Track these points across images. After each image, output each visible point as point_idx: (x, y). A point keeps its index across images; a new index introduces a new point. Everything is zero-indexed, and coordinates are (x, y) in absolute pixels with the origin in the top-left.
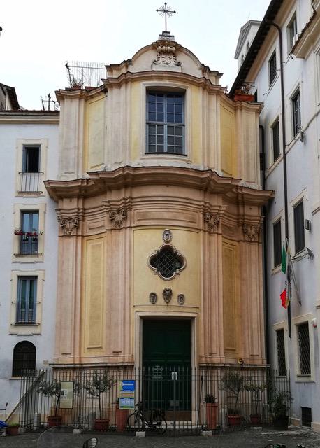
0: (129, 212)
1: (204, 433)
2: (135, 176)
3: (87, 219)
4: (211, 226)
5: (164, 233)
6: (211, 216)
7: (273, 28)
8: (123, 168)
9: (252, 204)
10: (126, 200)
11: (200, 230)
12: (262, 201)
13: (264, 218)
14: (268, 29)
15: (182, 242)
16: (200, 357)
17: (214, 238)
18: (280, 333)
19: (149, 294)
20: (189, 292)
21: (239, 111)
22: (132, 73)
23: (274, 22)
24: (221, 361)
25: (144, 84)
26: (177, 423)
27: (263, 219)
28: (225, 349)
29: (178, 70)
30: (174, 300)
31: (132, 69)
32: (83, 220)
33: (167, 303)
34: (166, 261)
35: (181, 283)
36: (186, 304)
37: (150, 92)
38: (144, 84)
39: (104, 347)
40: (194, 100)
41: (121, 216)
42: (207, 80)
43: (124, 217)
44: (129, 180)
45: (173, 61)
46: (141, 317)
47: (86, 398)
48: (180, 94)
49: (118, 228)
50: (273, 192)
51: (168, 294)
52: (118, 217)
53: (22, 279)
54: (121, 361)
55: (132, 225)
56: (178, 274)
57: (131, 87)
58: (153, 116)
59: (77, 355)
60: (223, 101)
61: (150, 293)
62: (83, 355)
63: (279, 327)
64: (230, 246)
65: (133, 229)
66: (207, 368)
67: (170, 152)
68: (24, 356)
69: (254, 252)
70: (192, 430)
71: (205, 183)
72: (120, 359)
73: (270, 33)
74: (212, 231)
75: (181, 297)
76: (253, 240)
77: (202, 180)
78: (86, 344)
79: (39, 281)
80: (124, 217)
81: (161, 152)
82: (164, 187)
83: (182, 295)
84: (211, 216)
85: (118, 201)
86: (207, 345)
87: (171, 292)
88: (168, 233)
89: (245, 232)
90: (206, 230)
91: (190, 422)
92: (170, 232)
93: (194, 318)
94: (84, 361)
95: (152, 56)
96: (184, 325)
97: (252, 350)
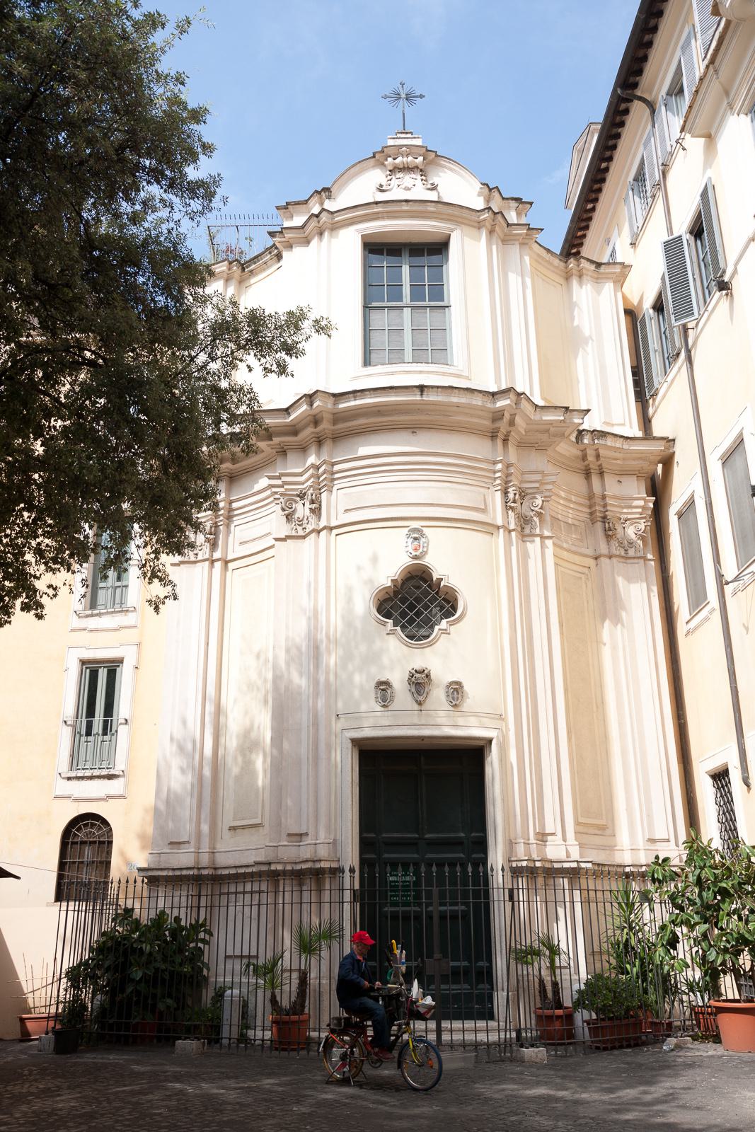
0: (324, 496)
1: (528, 1052)
2: (338, 418)
3: (236, 520)
4: (524, 521)
5: (408, 536)
6: (522, 498)
7: (637, 108)
8: (310, 398)
9: (623, 473)
10: (318, 468)
11: (498, 528)
12: (494, 247)
13: (656, 503)
14: (626, 112)
15: (449, 560)
16: (511, 844)
17: (534, 547)
18: (721, 777)
19: (373, 684)
20: (479, 679)
21: (575, 282)
22: (332, 213)
23: (638, 93)
24: (568, 855)
25: (358, 231)
26: (445, 1024)
27: (651, 505)
28: (577, 823)
29: (432, 196)
30: (438, 695)
31: (330, 205)
32: (228, 526)
33: (420, 703)
34: (416, 602)
35: (450, 653)
36: (468, 705)
37: (373, 247)
38: (358, 231)
39: (266, 824)
40: (469, 258)
41: (308, 505)
42: (495, 214)
43: (313, 506)
44: (325, 426)
45: (419, 182)
46: (355, 742)
47: (226, 957)
48: (439, 248)
49: (301, 533)
50: (671, 441)
51: (420, 683)
52: (302, 510)
53: (91, 669)
54: (191, 865)
55: (333, 524)
56: (445, 632)
57: (329, 241)
58: (374, 295)
59: (205, 848)
60: (537, 259)
61: (376, 680)
62: (220, 847)
63: (714, 764)
64: (575, 567)
65: (335, 532)
66: (531, 872)
67: (420, 355)
68: (85, 840)
69: (639, 596)
70: (488, 1045)
71: (499, 422)
72: (306, 853)
73: (631, 121)
74: (527, 531)
75: (456, 691)
76: (631, 552)
77: (497, 416)
78: (228, 819)
79: (125, 677)
80: (313, 506)
81: (395, 355)
82: (405, 435)
83: (387, 683)
84: (522, 498)
85: (301, 475)
86: (530, 813)
87: (428, 676)
88: (417, 535)
89: (609, 534)
90: (512, 526)
91: (492, 1024)
92: (422, 535)
93: (490, 741)
94: (222, 860)
95: (377, 176)
96: (461, 766)
97: (651, 826)
